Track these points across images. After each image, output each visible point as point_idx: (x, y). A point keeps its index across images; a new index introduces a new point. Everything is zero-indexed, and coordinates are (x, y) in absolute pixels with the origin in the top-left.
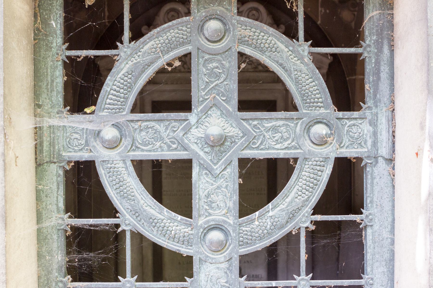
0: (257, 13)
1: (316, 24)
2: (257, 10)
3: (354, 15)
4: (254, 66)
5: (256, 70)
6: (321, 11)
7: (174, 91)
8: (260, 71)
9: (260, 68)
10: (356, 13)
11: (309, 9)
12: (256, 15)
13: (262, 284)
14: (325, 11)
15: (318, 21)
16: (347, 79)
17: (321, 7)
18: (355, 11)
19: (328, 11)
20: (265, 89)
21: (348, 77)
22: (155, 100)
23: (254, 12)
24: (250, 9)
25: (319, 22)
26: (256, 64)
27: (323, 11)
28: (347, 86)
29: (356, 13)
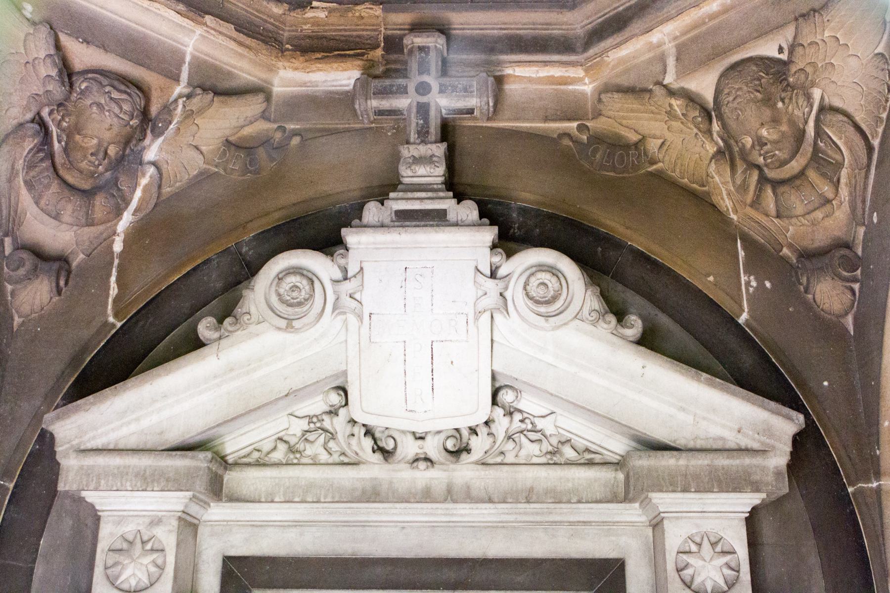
0: (554, 279)
1: (732, 321)
2: (553, 271)
3: (853, 291)
4: (550, 448)
5: (556, 459)
6: (748, 284)
7: (297, 524)
8: (570, 463)
9: (569, 453)
10: (856, 286)
11: (711, 278)
12: (550, 285)
13: (548, 72)
14: (761, 285)
15: (739, 317)
16: (850, 490)
17: (748, 272)
18: (855, 280)
19: (768, 284)
20: (585, 523)
21: (852, 484)
22: (233, 553)
23: (545, 277)
24: (534, 269)
25: (743, 319)
26: (554, 441)
27: (754, 284)
28: (853, 512)
29: (856, 286)
